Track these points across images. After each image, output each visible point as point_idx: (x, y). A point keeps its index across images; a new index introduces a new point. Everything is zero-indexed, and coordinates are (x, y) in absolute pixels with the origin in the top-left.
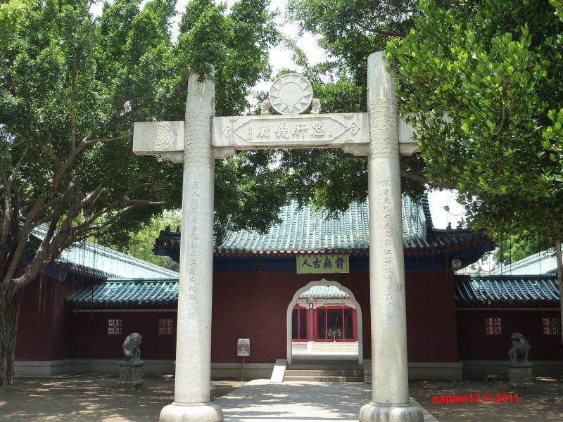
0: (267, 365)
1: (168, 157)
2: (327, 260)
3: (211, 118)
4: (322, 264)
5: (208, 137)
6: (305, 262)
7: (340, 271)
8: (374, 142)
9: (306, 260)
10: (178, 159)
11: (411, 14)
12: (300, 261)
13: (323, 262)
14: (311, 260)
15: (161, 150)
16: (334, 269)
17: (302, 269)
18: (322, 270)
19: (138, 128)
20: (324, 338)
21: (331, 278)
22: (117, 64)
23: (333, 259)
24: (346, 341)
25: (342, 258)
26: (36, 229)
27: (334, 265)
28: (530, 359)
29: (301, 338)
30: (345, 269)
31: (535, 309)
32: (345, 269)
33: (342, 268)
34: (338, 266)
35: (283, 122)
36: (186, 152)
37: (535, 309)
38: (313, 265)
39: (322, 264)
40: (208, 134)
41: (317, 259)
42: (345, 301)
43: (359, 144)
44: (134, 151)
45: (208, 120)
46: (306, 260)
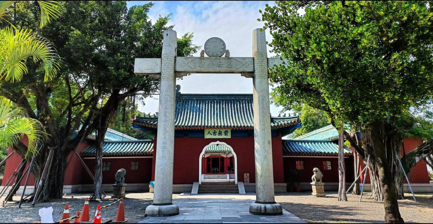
1: (153, 75)
2: (220, 131)
3: (175, 57)
4: (217, 134)
5: (173, 67)
7: (226, 137)
8: (256, 71)
10: (158, 76)
11: (380, 24)
12: (206, 132)
13: (218, 132)
14: (212, 131)
15: (149, 72)
16: (223, 136)
17: (207, 136)
18: (217, 137)
19: (138, 61)
22: (413, 48)
23: (223, 131)
27: (223, 134)
28: (323, 182)
29: (219, 158)
30: (229, 136)
32: (229, 136)
34: (225, 135)
35: (211, 60)
36: (162, 73)
38: (213, 134)
39: (217, 134)
40: (173, 65)
42: (221, 154)
43: (249, 72)
44: (135, 72)
45: (174, 58)
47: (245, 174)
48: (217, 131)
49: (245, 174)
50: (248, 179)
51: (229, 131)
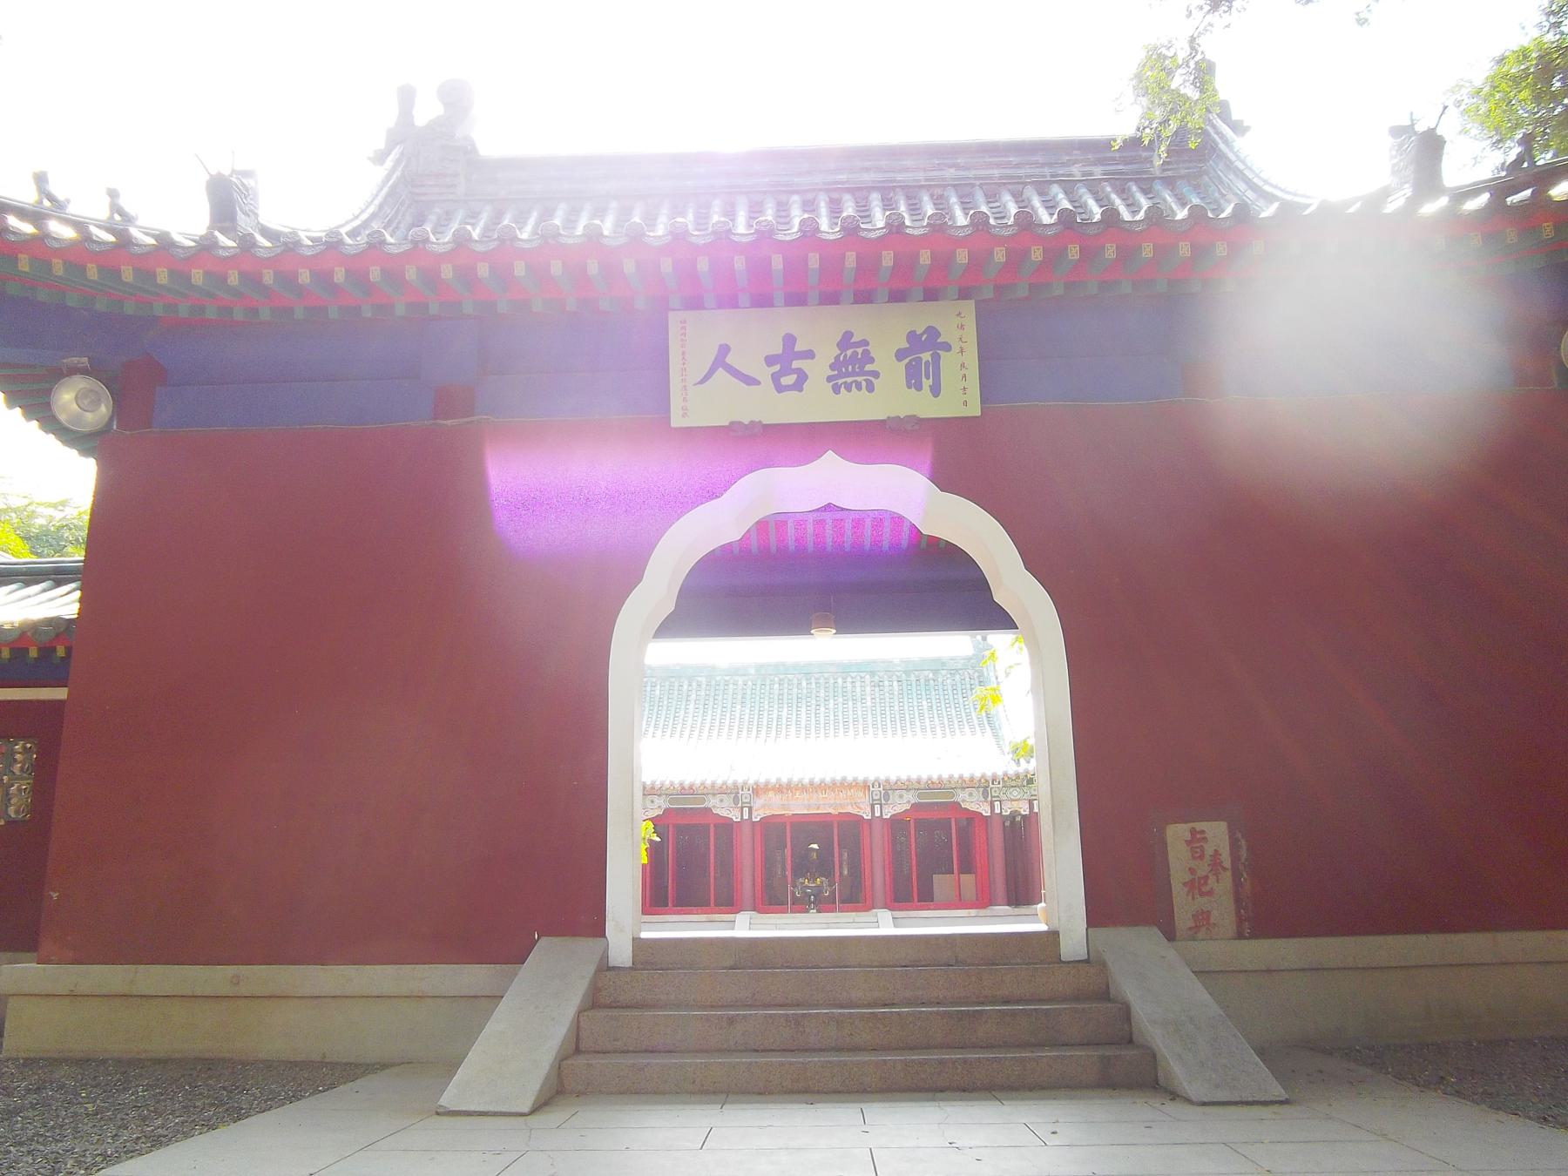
0: (474, 976)
2: (846, 341)
6: (721, 359)
7: (924, 406)
9: (724, 350)
13: (827, 353)
16: (890, 397)
18: (819, 403)
20: (784, 903)
21: (865, 439)
24: (841, 911)
25: (932, 332)
26: (78, 594)
27: (891, 372)
31: (883, 924)
32: (958, 395)
33: (936, 390)
37: (883, 924)
38: (764, 373)
39: (818, 370)
41: (789, 340)
46: (724, 350)
49: (1176, 834)
50: (1223, 886)
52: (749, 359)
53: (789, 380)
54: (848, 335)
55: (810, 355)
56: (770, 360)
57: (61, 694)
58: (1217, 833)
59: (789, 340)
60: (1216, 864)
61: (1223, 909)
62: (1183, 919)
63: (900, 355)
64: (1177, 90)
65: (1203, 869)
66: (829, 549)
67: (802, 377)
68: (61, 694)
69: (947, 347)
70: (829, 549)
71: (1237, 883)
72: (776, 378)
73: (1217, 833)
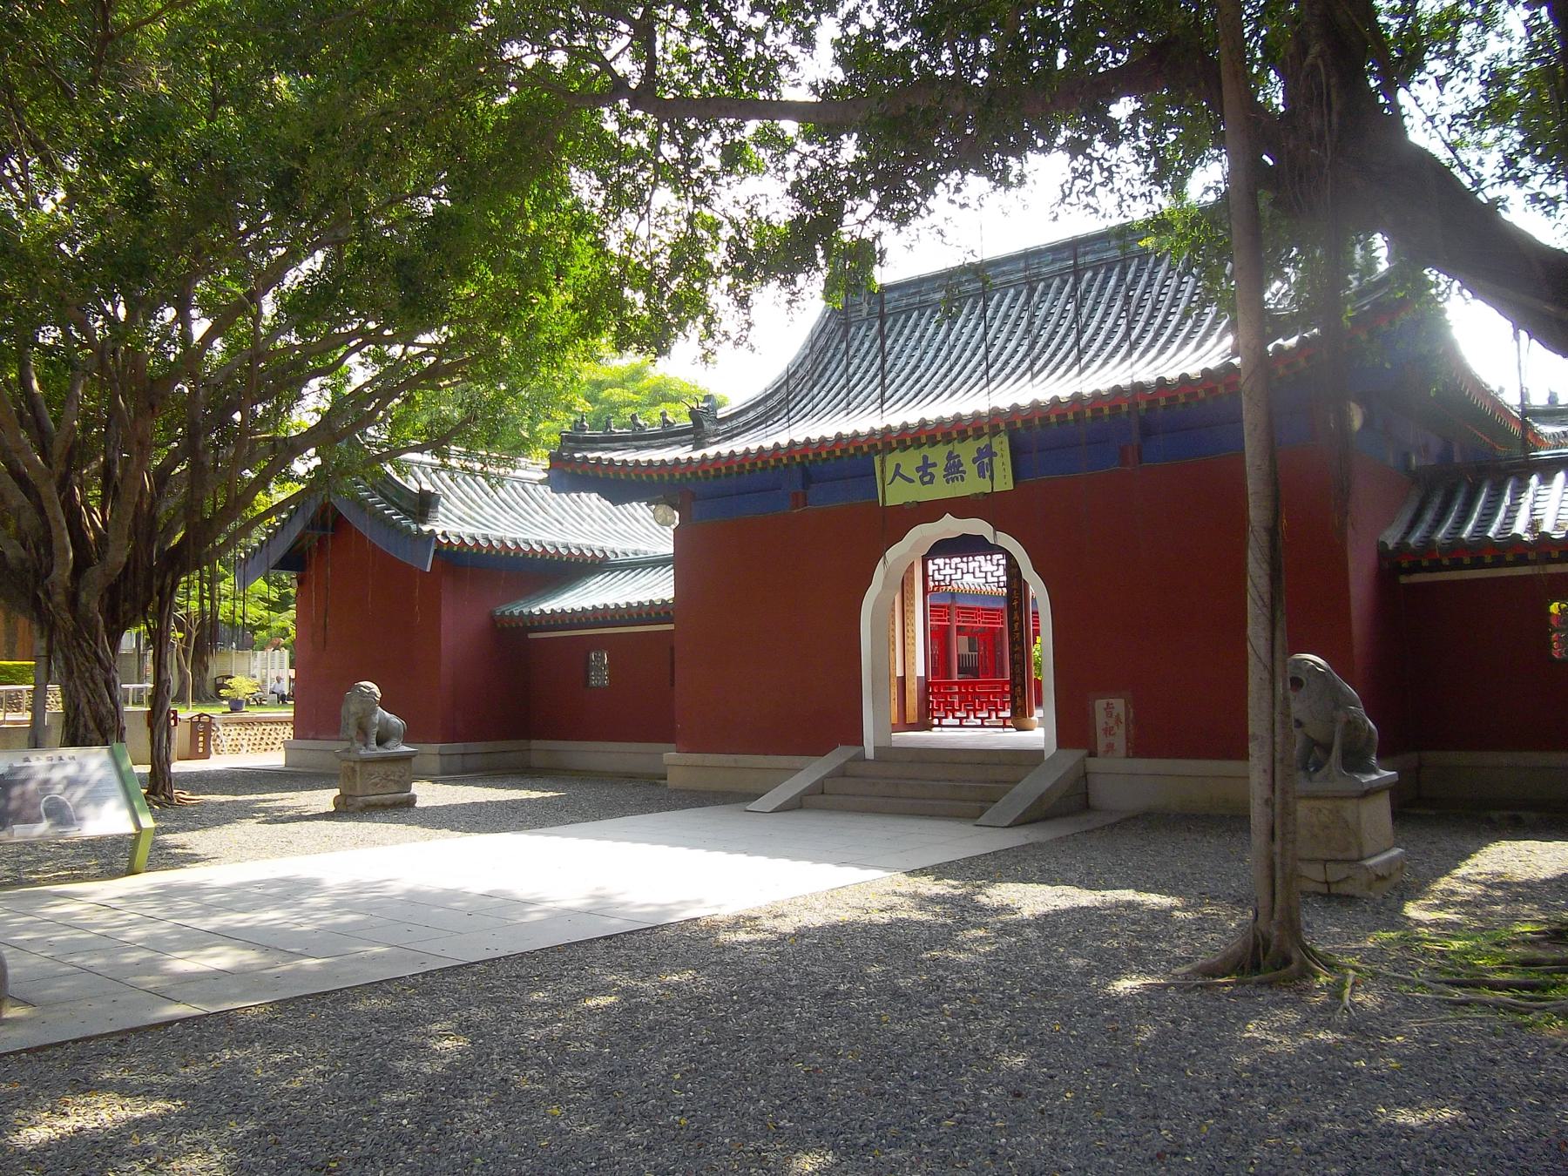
2: (950, 456)
4: (939, 472)
7: (984, 486)
9: (898, 466)
14: (909, 461)
16: (972, 484)
17: (896, 494)
27: (970, 469)
30: (1004, 481)
32: (1004, 481)
34: (981, 474)
38: (916, 476)
39: (939, 472)
41: (925, 458)
46: (898, 466)
47: (1100, 704)
48: (938, 454)
49: (1100, 704)
50: (1120, 732)
51: (1002, 446)
52: (909, 470)
53: (927, 479)
54: (950, 453)
55: (934, 465)
56: (918, 469)
57: (671, 627)
58: (1119, 705)
59: (925, 458)
60: (1118, 721)
61: (1120, 739)
62: (1101, 748)
63: (974, 461)
64: (312, 255)
65: (1111, 722)
66: (1391, 547)
67: (932, 476)
68: (671, 627)
69: (995, 454)
70: (1391, 547)
71: (1127, 731)
72: (921, 478)
73: (1119, 705)
